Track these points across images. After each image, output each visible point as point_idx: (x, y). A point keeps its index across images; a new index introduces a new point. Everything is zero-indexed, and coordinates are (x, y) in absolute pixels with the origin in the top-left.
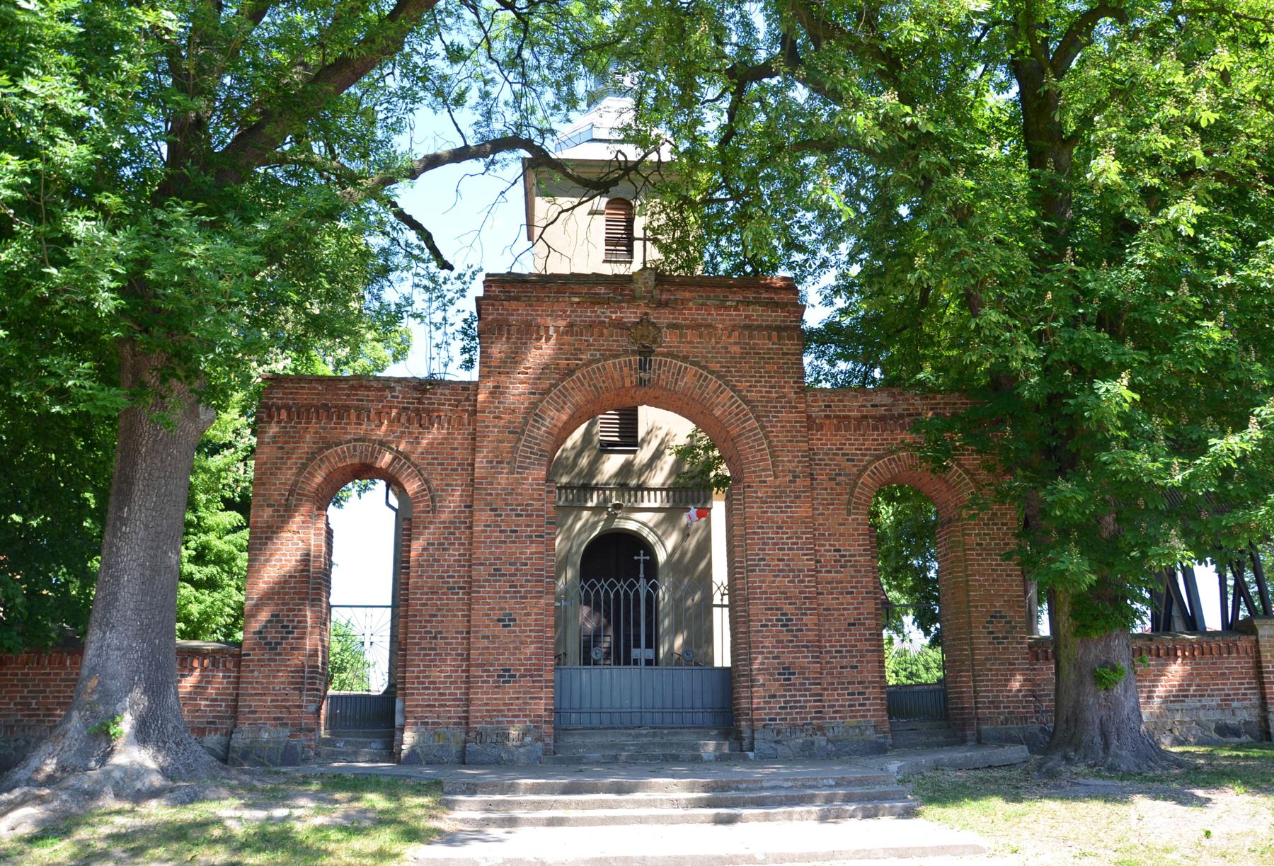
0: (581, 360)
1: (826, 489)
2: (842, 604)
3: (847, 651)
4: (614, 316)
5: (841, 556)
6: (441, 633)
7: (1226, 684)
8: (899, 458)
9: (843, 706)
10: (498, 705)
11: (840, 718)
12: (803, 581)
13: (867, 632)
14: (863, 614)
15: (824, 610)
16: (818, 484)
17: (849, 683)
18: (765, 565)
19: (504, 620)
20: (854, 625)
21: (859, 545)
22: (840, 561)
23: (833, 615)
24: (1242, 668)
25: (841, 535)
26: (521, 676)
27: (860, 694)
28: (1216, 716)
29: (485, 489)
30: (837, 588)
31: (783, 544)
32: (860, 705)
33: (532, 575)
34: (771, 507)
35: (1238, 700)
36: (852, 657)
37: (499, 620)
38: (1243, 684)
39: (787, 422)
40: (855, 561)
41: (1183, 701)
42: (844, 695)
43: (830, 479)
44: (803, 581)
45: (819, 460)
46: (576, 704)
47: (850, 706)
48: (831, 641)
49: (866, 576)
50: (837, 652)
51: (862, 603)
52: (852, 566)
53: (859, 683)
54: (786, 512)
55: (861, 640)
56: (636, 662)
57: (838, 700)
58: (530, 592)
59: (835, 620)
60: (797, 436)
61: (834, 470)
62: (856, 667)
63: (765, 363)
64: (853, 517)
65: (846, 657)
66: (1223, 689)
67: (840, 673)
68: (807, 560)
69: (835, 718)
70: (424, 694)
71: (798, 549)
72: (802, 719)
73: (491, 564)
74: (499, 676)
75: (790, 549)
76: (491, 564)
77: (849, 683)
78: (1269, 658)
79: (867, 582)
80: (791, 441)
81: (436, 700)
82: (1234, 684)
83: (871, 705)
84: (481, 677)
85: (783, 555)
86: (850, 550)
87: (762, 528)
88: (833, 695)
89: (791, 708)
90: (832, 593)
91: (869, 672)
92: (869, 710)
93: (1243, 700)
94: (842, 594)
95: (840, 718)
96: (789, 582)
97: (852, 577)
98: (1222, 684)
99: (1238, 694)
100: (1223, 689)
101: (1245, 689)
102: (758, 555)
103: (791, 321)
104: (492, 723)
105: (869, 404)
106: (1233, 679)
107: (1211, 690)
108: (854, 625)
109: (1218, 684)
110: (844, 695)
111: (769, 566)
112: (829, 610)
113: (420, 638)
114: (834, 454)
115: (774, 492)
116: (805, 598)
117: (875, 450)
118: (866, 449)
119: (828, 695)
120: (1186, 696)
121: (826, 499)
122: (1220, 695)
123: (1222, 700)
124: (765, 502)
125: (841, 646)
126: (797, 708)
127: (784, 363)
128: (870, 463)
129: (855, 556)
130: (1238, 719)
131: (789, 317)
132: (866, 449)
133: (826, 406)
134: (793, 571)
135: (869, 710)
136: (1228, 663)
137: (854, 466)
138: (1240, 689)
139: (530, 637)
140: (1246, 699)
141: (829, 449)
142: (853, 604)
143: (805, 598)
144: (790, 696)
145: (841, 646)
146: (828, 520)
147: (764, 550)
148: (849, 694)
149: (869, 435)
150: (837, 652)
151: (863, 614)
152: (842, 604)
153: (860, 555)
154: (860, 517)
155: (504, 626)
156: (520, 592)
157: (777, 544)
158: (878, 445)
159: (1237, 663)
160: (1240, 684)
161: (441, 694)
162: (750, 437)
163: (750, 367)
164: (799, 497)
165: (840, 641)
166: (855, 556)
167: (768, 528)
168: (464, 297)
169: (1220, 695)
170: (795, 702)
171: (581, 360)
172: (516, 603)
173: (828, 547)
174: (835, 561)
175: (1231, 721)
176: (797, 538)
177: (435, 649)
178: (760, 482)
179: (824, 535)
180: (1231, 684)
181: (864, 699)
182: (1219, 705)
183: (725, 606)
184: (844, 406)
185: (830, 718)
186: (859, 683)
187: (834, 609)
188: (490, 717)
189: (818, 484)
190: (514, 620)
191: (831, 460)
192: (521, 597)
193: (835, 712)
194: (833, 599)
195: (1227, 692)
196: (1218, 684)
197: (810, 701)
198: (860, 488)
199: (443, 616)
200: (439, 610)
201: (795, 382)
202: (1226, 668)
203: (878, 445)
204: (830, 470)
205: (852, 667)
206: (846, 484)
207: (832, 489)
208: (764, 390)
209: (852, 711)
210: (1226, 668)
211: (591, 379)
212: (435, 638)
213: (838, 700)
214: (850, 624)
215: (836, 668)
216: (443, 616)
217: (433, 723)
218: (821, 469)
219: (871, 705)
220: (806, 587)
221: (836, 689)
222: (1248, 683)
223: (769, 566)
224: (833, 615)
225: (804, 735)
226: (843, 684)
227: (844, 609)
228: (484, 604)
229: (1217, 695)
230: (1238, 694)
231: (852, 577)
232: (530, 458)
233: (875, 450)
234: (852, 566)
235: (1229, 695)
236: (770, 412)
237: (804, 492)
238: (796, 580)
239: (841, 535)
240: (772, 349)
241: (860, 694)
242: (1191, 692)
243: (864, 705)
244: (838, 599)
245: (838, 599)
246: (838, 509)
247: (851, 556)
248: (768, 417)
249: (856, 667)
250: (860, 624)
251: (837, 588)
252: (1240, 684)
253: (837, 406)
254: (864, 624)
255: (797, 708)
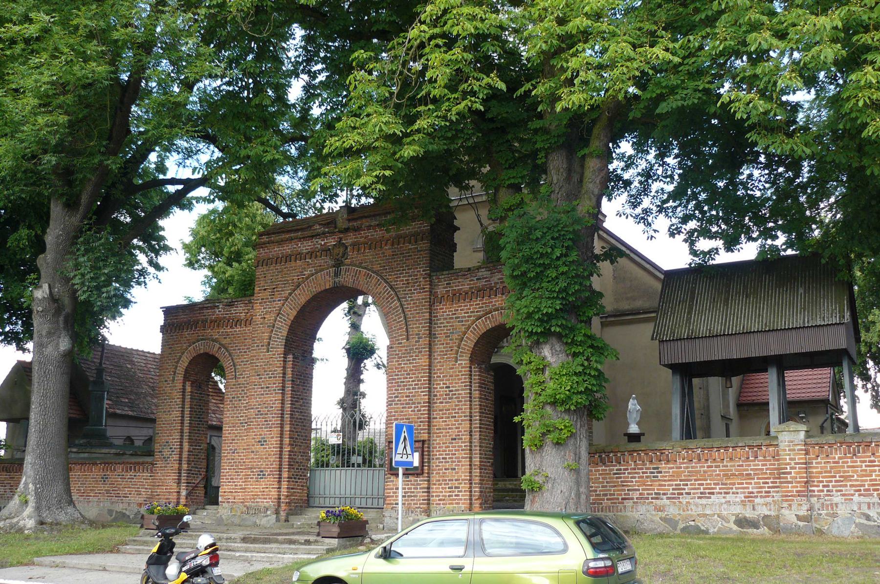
0: (304, 275)
1: (443, 344)
2: (449, 425)
3: (449, 458)
4: (323, 243)
5: (450, 391)
6: (236, 449)
7: (751, 483)
8: (492, 315)
9: (445, 496)
10: (257, 492)
11: (443, 504)
12: (420, 411)
13: (463, 445)
14: (461, 432)
15: (437, 429)
16: (438, 341)
17: (450, 480)
18: (398, 401)
19: (261, 442)
20: (455, 439)
21: (462, 383)
22: (449, 395)
23: (442, 433)
24: (767, 469)
25: (451, 376)
26: (268, 475)
27: (456, 488)
28: (738, 510)
29: (255, 363)
30: (446, 414)
31: (409, 385)
32: (455, 496)
33: (275, 414)
34: (404, 360)
35: (761, 497)
36: (452, 462)
37: (259, 442)
38: (767, 483)
39: (417, 300)
40: (459, 394)
41: (710, 498)
42: (446, 488)
43: (446, 337)
44: (420, 411)
45: (441, 323)
46: (322, 493)
47: (449, 496)
48: (439, 451)
49: (465, 405)
50: (443, 458)
51: (461, 424)
52: (456, 398)
53: (456, 480)
54: (413, 363)
55: (459, 450)
56: (353, 465)
57: (442, 492)
58: (274, 424)
59: (443, 436)
60: (422, 309)
61: (450, 330)
62: (455, 469)
63: (406, 260)
64: (459, 362)
65: (448, 462)
66: (748, 488)
67: (444, 473)
68: (424, 395)
69: (440, 504)
70: (228, 485)
71: (418, 388)
72: (414, 504)
73: (257, 408)
74: (258, 475)
75: (413, 389)
76: (257, 408)
77: (450, 480)
78: (788, 461)
79: (465, 409)
80: (418, 313)
81: (233, 489)
82: (759, 483)
83: (462, 495)
84: (250, 475)
85: (409, 393)
86: (456, 387)
87: (398, 375)
88: (439, 488)
89: (408, 496)
90: (442, 418)
91: (462, 472)
92: (461, 499)
93: (766, 497)
94: (449, 418)
95: (443, 504)
96: (412, 411)
97: (456, 405)
98: (747, 483)
99: (761, 492)
100: (748, 488)
101: (769, 487)
102: (394, 394)
103: (424, 227)
104: (254, 502)
105: (475, 279)
106: (758, 479)
107: (736, 488)
108: (455, 439)
109: (742, 484)
110: (446, 488)
111: (400, 401)
112: (440, 429)
113: (228, 453)
114: (450, 318)
115: (406, 350)
116: (421, 422)
117: (477, 312)
118: (471, 312)
119: (436, 488)
120: (713, 493)
121: (443, 351)
122: (744, 493)
123: (745, 497)
124: (400, 358)
125: (446, 454)
126: (412, 496)
127: (418, 258)
128: (474, 322)
129: (458, 390)
130: (756, 513)
131: (423, 224)
132: (471, 312)
133: (447, 284)
134: (414, 403)
135: (461, 499)
136: (754, 465)
137: (463, 325)
138: (764, 487)
139: (273, 451)
140: (768, 496)
141: (448, 315)
142: (455, 424)
143: (421, 422)
144: (408, 489)
145: (446, 454)
146: (443, 366)
147: (398, 390)
148: (449, 488)
149: (474, 302)
150: (443, 458)
151: (461, 432)
152: (449, 425)
153: (462, 390)
154: (463, 362)
155: (261, 445)
156: (269, 424)
157: (406, 385)
158: (479, 308)
159: (763, 465)
160: (764, 483)
161: (236, 485)
162: (284, 320)
163: (397, 264)
164: (420, 352)
165: (446, 451)
166: (458, 390)
167: (401, 375)
168: (617, 215)
169: (744, 493)
170: (411, 492)
171: (304, 275)
172: (267, 431)
173: (442, 386)
174: (446, 395)
175: (749, 514)
176: (418, 381)
177: (233, 459)
178: (399, 344)
179: (440, 377)
180: (756, 483)
181: (458, 491)
182: (742, 501)
183: (314, 429)
184: (459, 282)
185: (436, 504)
186: (456, 480)
187: (443, 429)
188: (254, 499)
189: (438, 341)
190: (266, 441)
191: (448, 322)
192: (270, 428)
193: (439, 500)
194: (443, 421)
195: (750, 490)
196: (742, 484)
197: (420, 492)
198: (465, 341)
199: (238, 440)
200: (236, 436)
201: (423, 271)
202: (752, 470)
203: (479, 308)
204: (447, 330)
205: (452, 469)
206: (456, 339)
207: (447, 344)
208: (404, 279)
209: (451, 500)
210: (752, 470)
211: (309, 287)
212: (234, 453)
213: (442, 492)
214: (452, 439)
215: (442, 470)
216: (238, 440)
217: (232, 502)
218: (441, 330)
219: (462, 495)
220: (421, 414)
221: (441, 484)
222: (772, 483)
223: (400, 401)
224: (442, 433)
225: (413, 515)
226: (446, 480)
227: (449, 428)
228: (253, 432)
229: (742, 493)
230: (761, 492)
231: (456, 405)
232: (277, 341)
233: (477, 312)
234: (456, 398)
235: (752, 493)
236: (407, 294)
237: (424, 348)
238: (416, 409)
239: (451, 376)
240: (411, 249)
241: (456, 488)
242: (718, 490)
243: (458, 495)
244: (446, 421)
245: (446, 421)
246: (450, 358)
247: (456, 390)
248: (406, 298)
249: (455, 469)
250: (459, 439)
251: (446, 414)
252: (764, 483)
253: (454, 283)
254: (462, 439)
255: (412, 496)
